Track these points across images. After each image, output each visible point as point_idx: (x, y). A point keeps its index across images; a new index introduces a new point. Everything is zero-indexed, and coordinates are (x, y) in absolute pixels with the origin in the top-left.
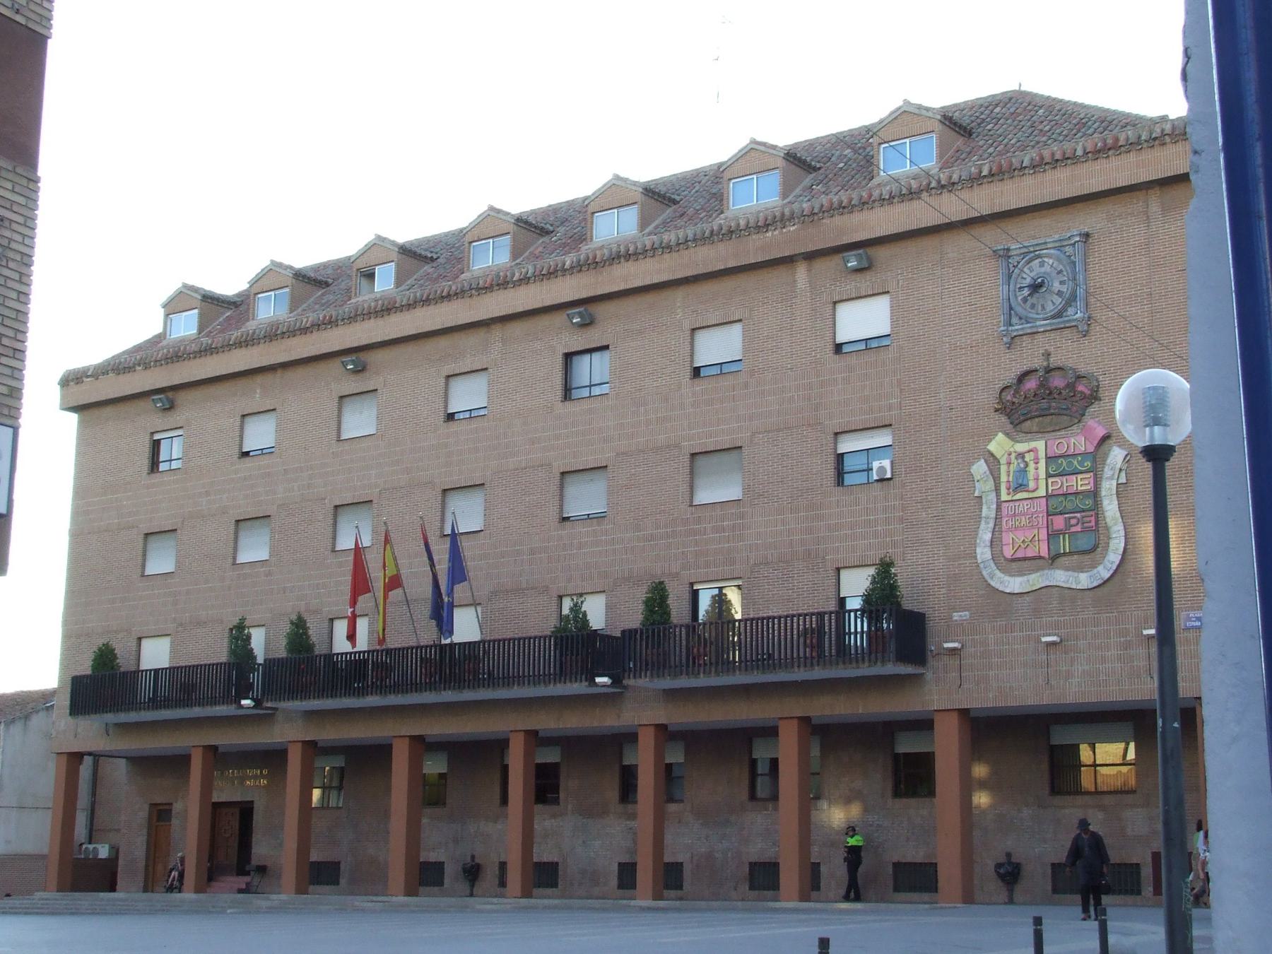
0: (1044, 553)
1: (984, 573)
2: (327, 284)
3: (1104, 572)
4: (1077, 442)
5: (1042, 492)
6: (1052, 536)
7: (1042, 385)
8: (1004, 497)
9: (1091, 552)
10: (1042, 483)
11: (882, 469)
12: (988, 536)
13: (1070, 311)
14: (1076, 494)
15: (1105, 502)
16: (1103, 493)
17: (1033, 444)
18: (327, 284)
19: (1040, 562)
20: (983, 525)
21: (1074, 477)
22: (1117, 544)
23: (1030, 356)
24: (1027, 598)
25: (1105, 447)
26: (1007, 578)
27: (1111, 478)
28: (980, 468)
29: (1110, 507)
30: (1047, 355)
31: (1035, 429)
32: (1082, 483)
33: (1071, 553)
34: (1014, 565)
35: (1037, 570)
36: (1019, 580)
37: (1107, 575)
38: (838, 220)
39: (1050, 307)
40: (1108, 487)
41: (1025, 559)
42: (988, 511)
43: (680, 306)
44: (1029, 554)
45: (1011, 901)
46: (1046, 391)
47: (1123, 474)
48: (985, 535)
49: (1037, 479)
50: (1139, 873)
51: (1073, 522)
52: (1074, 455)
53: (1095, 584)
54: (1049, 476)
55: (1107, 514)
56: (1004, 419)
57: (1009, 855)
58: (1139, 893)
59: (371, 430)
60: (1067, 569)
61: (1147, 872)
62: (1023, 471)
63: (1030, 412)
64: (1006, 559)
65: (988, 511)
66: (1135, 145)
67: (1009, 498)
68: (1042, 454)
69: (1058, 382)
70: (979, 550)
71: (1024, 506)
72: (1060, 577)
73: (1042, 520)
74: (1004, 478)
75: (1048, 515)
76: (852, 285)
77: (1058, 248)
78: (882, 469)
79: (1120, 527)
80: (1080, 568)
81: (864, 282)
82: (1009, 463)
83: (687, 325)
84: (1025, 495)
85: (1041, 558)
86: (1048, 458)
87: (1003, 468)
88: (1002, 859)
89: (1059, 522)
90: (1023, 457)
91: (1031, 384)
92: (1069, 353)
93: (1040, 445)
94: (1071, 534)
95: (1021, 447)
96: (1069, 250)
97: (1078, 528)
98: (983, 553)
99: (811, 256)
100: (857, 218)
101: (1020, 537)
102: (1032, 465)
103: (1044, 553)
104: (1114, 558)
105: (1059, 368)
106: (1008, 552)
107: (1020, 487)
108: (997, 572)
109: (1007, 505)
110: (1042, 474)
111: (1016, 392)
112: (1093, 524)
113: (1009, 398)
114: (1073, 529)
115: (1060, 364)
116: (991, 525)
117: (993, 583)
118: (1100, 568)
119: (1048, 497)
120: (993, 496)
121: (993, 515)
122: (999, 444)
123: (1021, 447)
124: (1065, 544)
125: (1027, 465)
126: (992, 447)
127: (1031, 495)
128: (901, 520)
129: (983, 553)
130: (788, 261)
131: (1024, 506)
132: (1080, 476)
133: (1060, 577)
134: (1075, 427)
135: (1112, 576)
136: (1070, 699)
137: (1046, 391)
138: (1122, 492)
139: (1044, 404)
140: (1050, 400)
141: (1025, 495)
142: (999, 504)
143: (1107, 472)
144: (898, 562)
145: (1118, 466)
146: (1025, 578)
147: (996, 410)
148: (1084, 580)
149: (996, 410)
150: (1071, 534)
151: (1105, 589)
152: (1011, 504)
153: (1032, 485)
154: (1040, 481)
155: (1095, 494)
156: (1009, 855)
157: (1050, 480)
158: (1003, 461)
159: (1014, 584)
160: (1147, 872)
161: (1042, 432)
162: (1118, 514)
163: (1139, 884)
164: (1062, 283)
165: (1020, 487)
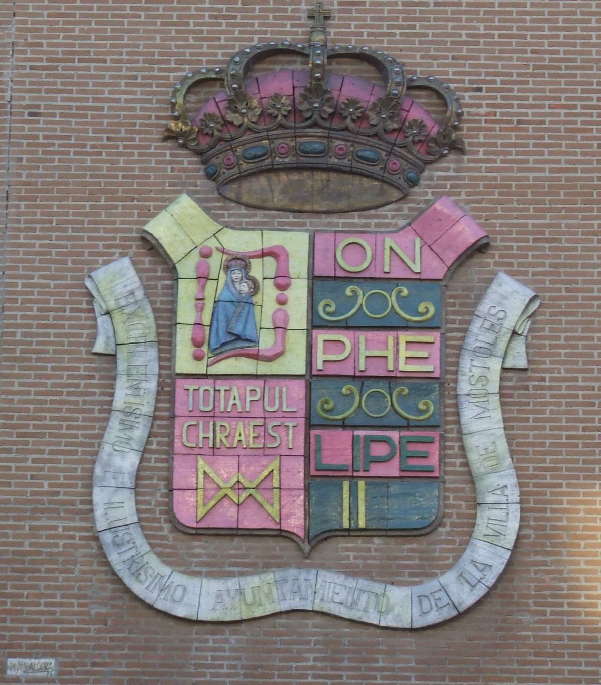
0: (295, 522)
1: (115, 558)
2: (486, 245)
3: (460, 589)
4: (394, 247)
5: (294, 362)
6: (321, 481)
7: (316, 90)
8: (184, 362)
9: (414, 537)
10: (297, 343)
12: (129, 462)
14: (391, 380)
15: (469, 412)
16: (464, 387)
17: (273, 239)
18: (486, 245)
19: (278, 546)
21: (390, 337)
22: (500, 519)
24: (234, 639)
25: (473, 272)
26: (178, 579)
27: (488, 351)
28: (117, 279)
29: (483, 427)
30: (320, 17)
31: (278, 199)
32: (404, 354)
33: (367, 533)
34: (199, 546)
36: (213, 586)
37: (467, 597)
41: (233, 533)
42: (135, 393)
44: (252, 521)
46: (319, 110)
47: (519, 346)
48: (120, 457)
49: (281, 328)
51: (379, 450)
52: (389, 281)
53: (433, 618)
54: (315, 324)
55: (472, 442)
56: (188, 162)
60: (351, 571)
62: (245, 304)
63: (270, 153)
64: (178, 527)
65: (135, 393)
67: (200, 368)
68: (298, 266)
69: (353, 88)
70: (99, 496)
71: (237, 395)
72: (330, 590)
73: (293, 438)
74: (186, 313)
75: (310, 425)
79: (509, 479)
80: (389, 574)
82: (203, 278)
84: (245, 366)
85: (281, 534)
86: (314, 279)
87: (186, 290)
89: (338, 448)
90: (246, 267)
91: (279, 84)
93: (296, 243)
94: (373, 482)
97: (392, 469)
98: (114, 504)
101: (225, 472)
102: (269, 292)
103: (295, 522)
104: (487, 556)
105: (440, 96)
106: (189, 508)
107: (238, 342)
108: (153, 561)
109: (191, 385)
111: (237, 100)
112: (434, 461)
113: (211, 108)
114: (377, 470)
115: (353, 43)
116: (139, 433)
117: (137, 589)
118: (449, 578)
119: (312, 378)
120: (148, 359)
121: (146, 405)
122: (181, 224)
124: (354, 507)
125: (255, 287)
126: (160, 228)
127: (264, 368)
129: (114, 504)
131: (237, 395)
132: (404, 337)
133: (330, 590)
134: (386, 210)
135: (479, 603)
137: (319, 110)
138: (514, 386)
139: (313, 140)
141: (245, 366)
142: (168, 383)
143: (478, 335)
145: (509, 324)
146: (232, 583)
147: (170, 136)
149: (170, 136)
150: (373, 482)
151: (458, 636)
152: (207, 385)
153: (266, 341)
155: (441, 385)
157: (321, 337)
158: (187, 269)
159: (200, 597)
161: (296, 211)
162: (502, 446)
165: (238, 342)
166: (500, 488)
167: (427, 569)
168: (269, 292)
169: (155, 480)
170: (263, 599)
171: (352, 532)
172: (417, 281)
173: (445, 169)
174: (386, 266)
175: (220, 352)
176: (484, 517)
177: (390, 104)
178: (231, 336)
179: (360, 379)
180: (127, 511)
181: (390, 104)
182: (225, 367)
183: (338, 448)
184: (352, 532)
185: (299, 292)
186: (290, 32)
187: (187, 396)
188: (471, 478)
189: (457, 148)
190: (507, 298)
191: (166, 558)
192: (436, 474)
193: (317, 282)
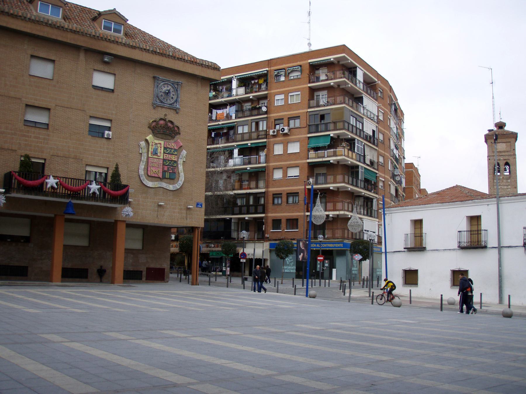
0: (161, 177)
4: (172, 144)
6: (164, 172)
8: (150, 156)
10: (162, 155)
11: (108, 134)
12: (143, 167)
13: (175, 104)
14: (172, 161)
15: (179, 166)
17: (160, 142)
20: (141, 163)
23: (160, 114)
27: (181, 159)
28: (143, 143)
29: (181, 167)
32: (173, 158)
34: (150, 178)
35: (157, 181)
36: (151, 183)
37: (179, 187)
38: (105, 44)
39: (169, 101)
40: (180, 162)
43: (28, 48)
45: (101, 281)
46: (166, 127)
48: (142, 166)
49: (160, 153)
50: (142, 274)
54: (164, 153)
56: (150, 131)
57: (101, 267)
58: (141, 279)
59: (299, 151)
61: (144, 273)
62: (157, 149)
65: (144, 158)
66: (174, 57)
68: (163, 145)
71: (155, 160)
74: (150, 150)
76: (101, 67)
77: (173, 84)
78: (108, 134)
81: (106, 69)
82: (152, 145)
83: (30, 52)
85: (159, 178)
87: (150, 147)
88: (100, 268)
92: (171, 116)
95: (157, 142)
96: (176, 86)
97: (171, 171)
98: (142, 172)
99: (88, 51)
100: (112, 45)
102: (159, 148)
103: (161, 177)
110: (162, 152)
119: (164, 160)
120: (146, 155)
121: (145, 160)
122: (150, 137)
123: (157, 142)
128: (113, 154)
129: (142, 172)
130: (77, 48)
131: (155, 160)
133: (164, 185)
136: (164, 223)
137: (166, 127)
140: (166, 130)
142: (148, 158)
143: (181, 157)
144: (31, 154)
148: (171, 187)
153: (159, 154)
154: (161, 151)
156: (101, 267)
158: (150, 144)
159: (150, 184)
160: (144, 273)
163: (142, 277)
164: (173, 95)
166: (182, 174)
167: (173, 184)
168: (159, 148)
169: (147, 169)
170: (209, 249)
171: (167, 178)
172: (175, 149)
173: (178, 136)
174: (172, 147)
175: (154, 155)
176: (180, 178)
177: (174, 127)
178: (155, 153)
179: (169, 160)
180: (143, 173)
181: (174, 127)
182: (383, 250)
183: (166, 169)
184: (167, 178)
185: (163, 148)
186: (163, 117)
187: (151, 160)
188: (179, 173)
189: (180, 134)
190: (184, 153)
191: (147, 179)
192: (313, 287)
193: (165, 148)
